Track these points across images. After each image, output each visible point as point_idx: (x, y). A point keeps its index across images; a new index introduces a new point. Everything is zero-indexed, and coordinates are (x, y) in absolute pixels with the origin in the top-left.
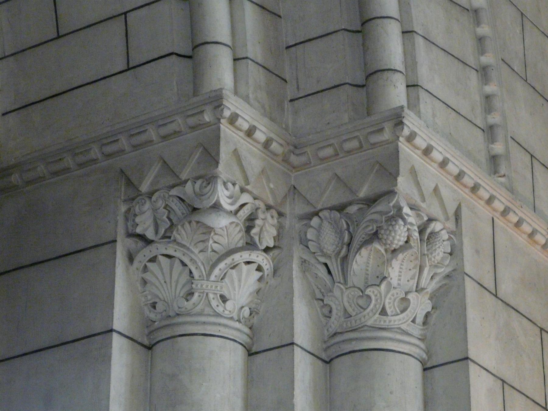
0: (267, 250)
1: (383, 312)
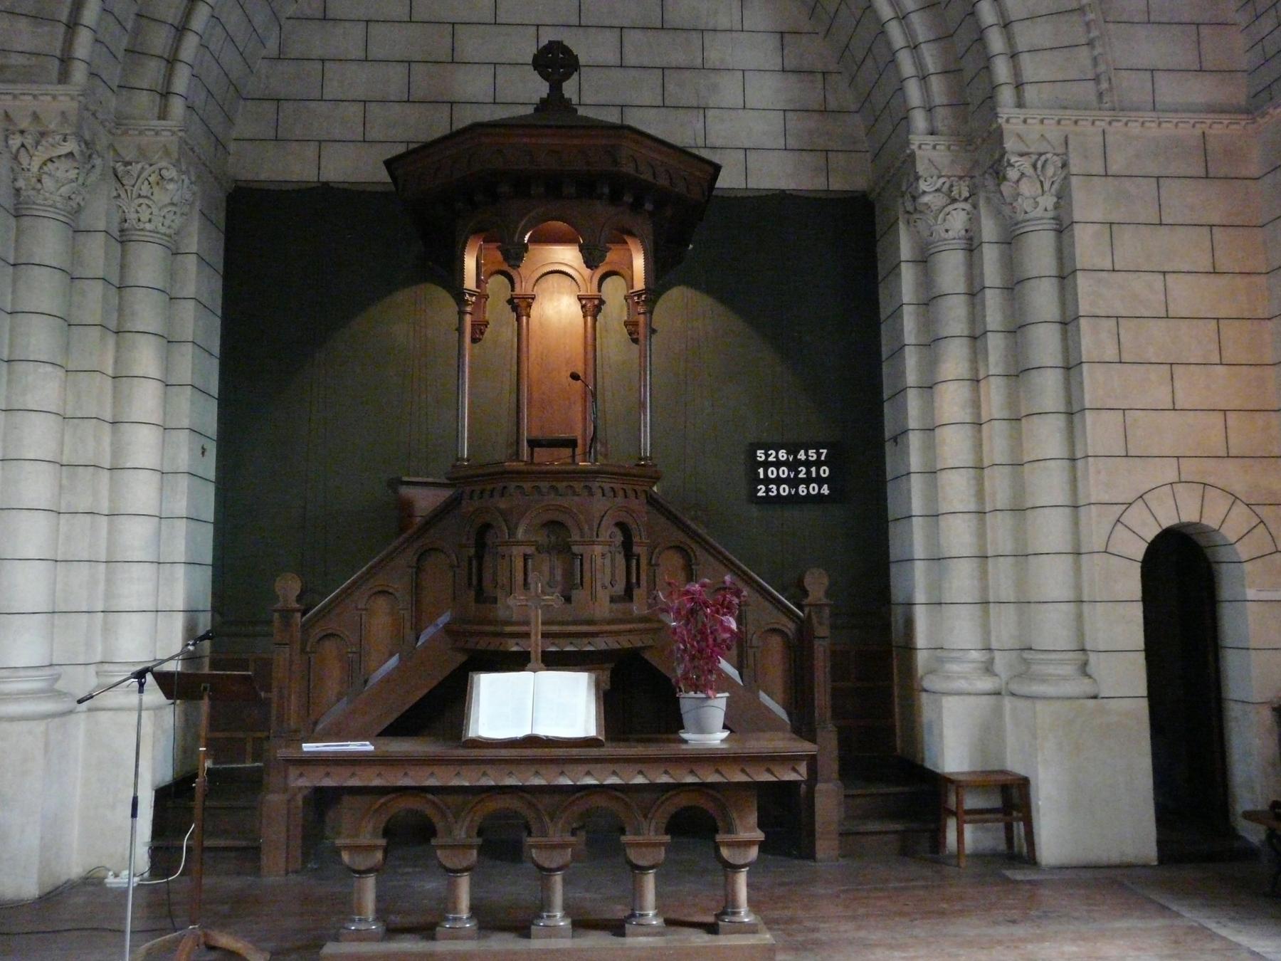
0: (966, 200)
1: (1026, 213)
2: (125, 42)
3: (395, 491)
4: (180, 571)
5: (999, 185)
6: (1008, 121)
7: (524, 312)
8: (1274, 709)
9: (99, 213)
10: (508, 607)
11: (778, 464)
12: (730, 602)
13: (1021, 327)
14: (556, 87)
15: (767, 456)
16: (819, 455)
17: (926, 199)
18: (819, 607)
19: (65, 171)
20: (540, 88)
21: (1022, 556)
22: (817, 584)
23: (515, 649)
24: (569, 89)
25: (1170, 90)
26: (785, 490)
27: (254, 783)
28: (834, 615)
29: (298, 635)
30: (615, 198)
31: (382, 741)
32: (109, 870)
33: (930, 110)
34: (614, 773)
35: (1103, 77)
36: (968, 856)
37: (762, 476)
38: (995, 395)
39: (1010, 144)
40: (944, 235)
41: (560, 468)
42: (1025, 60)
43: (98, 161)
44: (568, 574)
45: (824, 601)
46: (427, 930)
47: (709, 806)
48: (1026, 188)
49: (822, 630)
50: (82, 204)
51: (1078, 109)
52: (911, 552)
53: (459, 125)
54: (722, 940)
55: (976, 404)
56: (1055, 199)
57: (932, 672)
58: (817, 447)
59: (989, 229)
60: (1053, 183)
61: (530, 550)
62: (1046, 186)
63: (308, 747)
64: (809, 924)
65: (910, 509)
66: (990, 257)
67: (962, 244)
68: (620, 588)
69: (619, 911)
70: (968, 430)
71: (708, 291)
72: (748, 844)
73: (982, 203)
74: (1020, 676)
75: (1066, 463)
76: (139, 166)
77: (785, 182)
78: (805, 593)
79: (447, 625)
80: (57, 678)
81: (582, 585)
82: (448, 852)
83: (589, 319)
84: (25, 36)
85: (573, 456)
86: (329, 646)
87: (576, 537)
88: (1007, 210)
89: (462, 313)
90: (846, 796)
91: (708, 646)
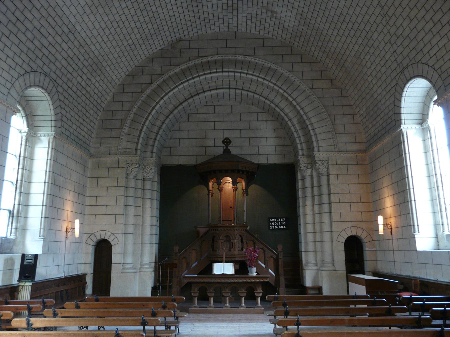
8: (372, 273)
11: (274, 222)
14: (227, 147)
15: (272, 220)
16: (283, 220)
17: (302, 168)
19: (135, 170)
22: (280, 247)
25: (349, 147)
26: (276, 227)
38: (316, 208)
39: (316, 159)
40: (306, 175)
42: (319, 142)
48: (321, 167)
56: (327, 169)
58: (283, 218)
59: (315, 174)
61: (222, 241)
62: (325, 167)
66: (315, 180)
70: (311, 215)
73: (313, 169)
77: (276, 161)
83: (235, 192)
84: (129, 146)
87: (231, 238)
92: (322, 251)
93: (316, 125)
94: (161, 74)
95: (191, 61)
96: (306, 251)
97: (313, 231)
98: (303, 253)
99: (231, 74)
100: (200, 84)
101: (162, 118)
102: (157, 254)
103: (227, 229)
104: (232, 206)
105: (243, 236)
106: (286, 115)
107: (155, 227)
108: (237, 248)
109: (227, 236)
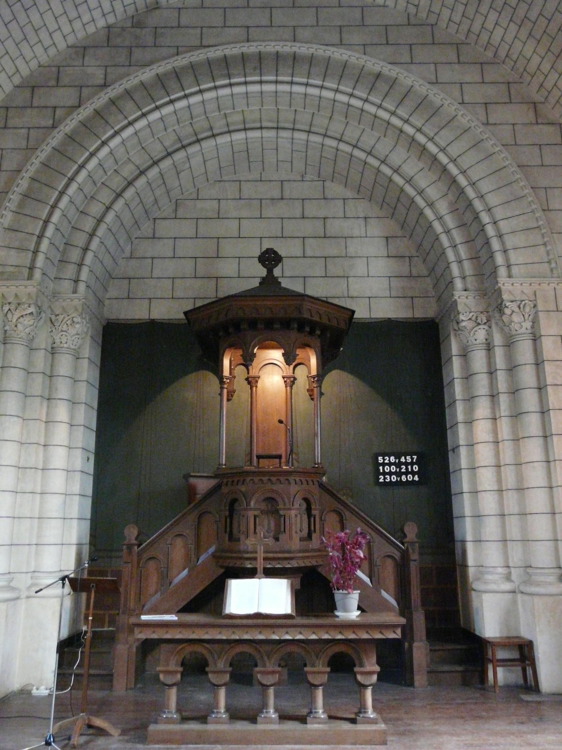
0: (485, 324)
1: (516, 331)
2: (58, 257)
3: (187, 481)
4: (75, 523)
5: (501, 316)
6: (503, 284)
7: (254, 385)
9: (42, 341)
10: (246, 544)
11: (390, 464)
12: (360, 543)
13: (517, 390)
14: (270, 271)
15: (384, 460)
16: (412, 459)
17: (463, 324)
18: (412, 543)
19: (28, 321)
20: (263, 272)
21: (523, 514)
23: (249, 566)
24: (277, 272)
26: (394, 478)
27: (111, 638)
28: (421, 547)
29: (135, 558)
30: (300, 329)
31: (180, 614)
32: (33, 686)
33: (464, 278)
34: (300, 633)
35: (553, 262)
36: (500, 687)
37: (381, 471)
39: (505, 296)
40: (475, 342)
41: (274, 470)
43: (43, 315)
44: (278, 525)
45: (416, 540)
46: (203, 719)
47: (350, 652)
48: (516, 318)
49: (414, 556)
50: (35, 336)
51: (540, 277)
52: (464, 513)
53: (221, 295)
54: (360, 727)
55: (495, 431)
56: (531, 324)
57: (477, 579)
59: (498, 339)
60: (529, 315)
61: (256, 513)
62: (526, 316)
63: (144, 617)
64: (409, 722)
65: (462, 488)
66: (499, 353)
67: (484, 346)
68: (305, 532)
69: (305, 711)
70: (491, 446)
71: (352, 372)
72: (371, 673)
74: (525, 582)
75: (544, 464)
76: (62, 316)
77: (392, 315)
78: (405, 536)
79: (213, 553)
80: (11, 580)
81: (285, 532)
82: (216, 675)
83: (288, 388)
84: (14, 258)
85: (280, 463)
86: (152, 564)
87: (281, 506)
88: (507, 330)
89: (222, 388)
90: (431, 650)
91: (348, 566)
92: (525, 541)
93: (499, 213)
94: (105, 85)
95: (183, 56)
96: (478, 541)
97: (496, 488)
98: (470, 547)
99: (281, 88)
100: (204, 117)
101: (105, 196)
102: (86, 549)
103: (269, 480)
104: (283, 419)
105: (312, 500)
106: (421, 193)
107: (78, 477)
108: (296, 532)
109: (271, 500)
